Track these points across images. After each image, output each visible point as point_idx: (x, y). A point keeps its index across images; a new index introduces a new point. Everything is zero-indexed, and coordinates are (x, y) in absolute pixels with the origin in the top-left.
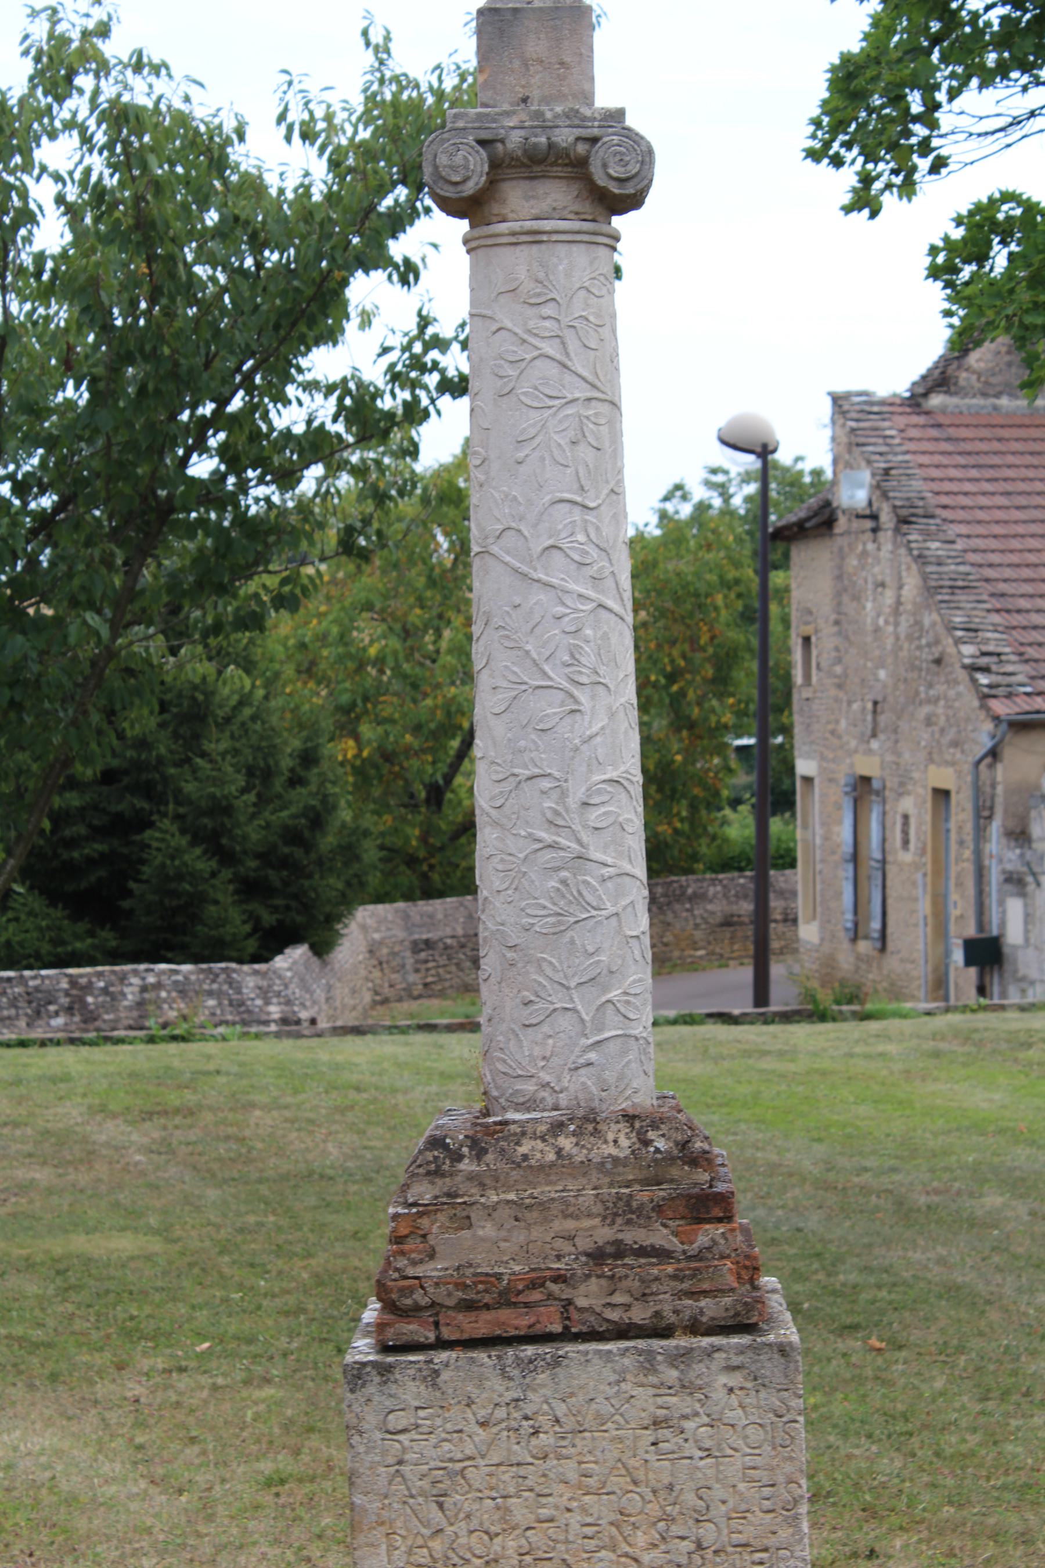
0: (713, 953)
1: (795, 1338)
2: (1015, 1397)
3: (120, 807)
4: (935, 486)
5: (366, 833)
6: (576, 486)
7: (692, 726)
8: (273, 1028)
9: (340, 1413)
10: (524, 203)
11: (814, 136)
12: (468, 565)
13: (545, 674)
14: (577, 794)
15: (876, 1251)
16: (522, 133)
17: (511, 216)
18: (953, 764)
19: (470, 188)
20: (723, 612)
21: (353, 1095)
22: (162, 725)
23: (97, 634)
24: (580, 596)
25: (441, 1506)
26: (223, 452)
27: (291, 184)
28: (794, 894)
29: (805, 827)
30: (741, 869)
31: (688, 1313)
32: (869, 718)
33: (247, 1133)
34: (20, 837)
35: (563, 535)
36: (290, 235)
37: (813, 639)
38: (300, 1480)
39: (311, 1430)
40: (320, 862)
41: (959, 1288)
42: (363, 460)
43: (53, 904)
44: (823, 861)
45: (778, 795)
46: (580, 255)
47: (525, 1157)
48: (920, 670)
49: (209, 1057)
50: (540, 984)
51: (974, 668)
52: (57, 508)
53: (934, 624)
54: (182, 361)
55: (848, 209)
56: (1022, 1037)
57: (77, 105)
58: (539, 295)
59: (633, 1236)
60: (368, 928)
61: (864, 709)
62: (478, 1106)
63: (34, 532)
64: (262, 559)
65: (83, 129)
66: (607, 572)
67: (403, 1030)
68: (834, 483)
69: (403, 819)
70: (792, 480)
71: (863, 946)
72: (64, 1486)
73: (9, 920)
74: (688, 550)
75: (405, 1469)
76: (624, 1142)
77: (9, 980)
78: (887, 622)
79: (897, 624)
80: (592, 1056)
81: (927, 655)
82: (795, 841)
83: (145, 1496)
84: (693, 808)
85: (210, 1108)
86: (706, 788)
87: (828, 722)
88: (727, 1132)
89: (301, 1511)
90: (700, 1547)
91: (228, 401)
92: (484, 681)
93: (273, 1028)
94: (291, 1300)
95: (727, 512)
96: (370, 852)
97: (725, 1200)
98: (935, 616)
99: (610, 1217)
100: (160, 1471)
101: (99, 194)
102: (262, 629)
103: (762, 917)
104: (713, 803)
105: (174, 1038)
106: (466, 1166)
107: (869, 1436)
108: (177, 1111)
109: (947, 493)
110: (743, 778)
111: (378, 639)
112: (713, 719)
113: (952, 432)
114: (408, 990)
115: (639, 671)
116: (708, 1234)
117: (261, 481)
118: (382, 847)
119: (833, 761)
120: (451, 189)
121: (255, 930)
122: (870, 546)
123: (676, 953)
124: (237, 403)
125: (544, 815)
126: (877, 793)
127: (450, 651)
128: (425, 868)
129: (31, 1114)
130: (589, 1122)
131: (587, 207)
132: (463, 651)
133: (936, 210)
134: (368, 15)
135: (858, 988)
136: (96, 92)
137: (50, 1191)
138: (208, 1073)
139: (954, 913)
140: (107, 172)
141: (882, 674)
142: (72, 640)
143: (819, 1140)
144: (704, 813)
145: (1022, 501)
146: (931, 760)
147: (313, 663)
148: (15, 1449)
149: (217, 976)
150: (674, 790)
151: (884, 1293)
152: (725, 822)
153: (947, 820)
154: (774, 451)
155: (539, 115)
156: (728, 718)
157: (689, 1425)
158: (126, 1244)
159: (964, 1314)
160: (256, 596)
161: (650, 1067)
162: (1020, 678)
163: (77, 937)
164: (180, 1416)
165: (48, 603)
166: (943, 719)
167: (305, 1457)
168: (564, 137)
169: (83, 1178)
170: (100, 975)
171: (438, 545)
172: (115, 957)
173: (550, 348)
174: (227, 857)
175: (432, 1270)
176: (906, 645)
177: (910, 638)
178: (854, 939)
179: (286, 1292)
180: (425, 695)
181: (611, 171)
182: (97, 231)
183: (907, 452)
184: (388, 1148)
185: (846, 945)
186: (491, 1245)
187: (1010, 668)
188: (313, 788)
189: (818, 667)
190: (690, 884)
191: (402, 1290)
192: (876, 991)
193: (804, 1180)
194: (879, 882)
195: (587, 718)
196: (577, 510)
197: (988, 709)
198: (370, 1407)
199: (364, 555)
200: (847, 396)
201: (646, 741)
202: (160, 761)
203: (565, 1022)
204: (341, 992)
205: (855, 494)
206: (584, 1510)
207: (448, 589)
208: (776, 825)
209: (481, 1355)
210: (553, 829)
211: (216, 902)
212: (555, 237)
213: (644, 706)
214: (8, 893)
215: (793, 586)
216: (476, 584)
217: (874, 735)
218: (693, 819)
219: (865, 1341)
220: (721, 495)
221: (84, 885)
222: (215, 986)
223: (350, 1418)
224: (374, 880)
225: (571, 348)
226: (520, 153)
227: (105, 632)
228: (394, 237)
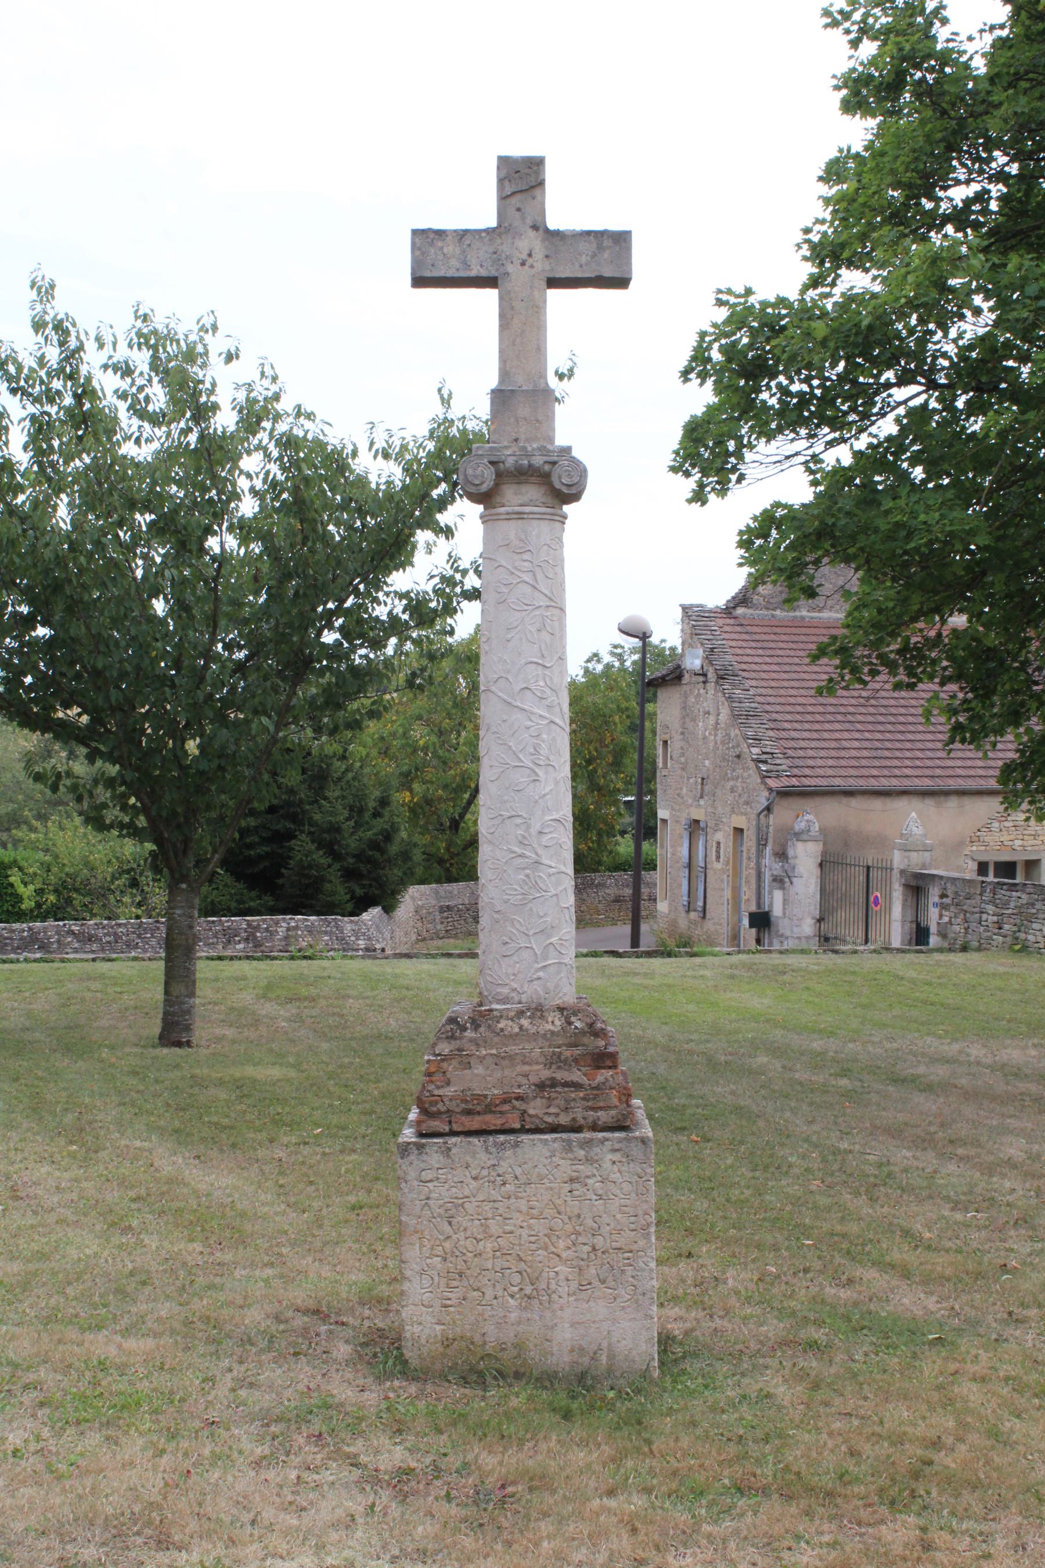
1: (650, 1134)
2: (771, 1170)
3: (278, 827)
4: (739, 659)
5: (415, 845)
7: (599, 789)
8: (361, 953)
9: (395, 1170)
10: (513, 496)
11: (675, 460)
12: (477, 696)
15: (696, 1086)
18: (746, 814)
19: (484, 488)
21: (404, 992)
25: (450, 1223)
26: (341, 629)
29: (662, 847)
30: (625, 870)
31: (590, 1120)
33: (345, 1011)
34: (221, 842)
36: (381, 509)
38: (371, 1207)
39: (377, 1179)
40: (389, 861)
41: (741, 1108)
42: (419, 636)
43: (238, 880)
45: (647, 829)
46: (544, 527)
47: (502, 1030)
49: (324, 969)
52: (248, 658)
55: (690, 501)
56: (781, 968)
57: (263, 436)
59: (561, 1075)
60: (415, 898)
62: (476, 1000)
63: (235, 672)
64: (361, 689)
65: (265, 449)
67: (433, 956)
68: (682, 655)
69: (437, 838)
70: (659, 653)
71: (693, 915)
72: (239, 1206)
75: (431, 1202)
76: (558, 1023)
79: (716, 735)
80: (541, 974)
83: (284, 1213)
84: (599, 835)
85: (325, 997)
86: (606, 823)
88: (615, 1018)
89: (371, 1224)
90: (594, 1249)
91: (345, 601)
92: (485, 762)
93: (361, 953)
94: (368, 1106)
95: (623, 670)
96: (417, 856)
97: (613, 1056)
98: (737, 731)
99: (548, 1065)
100: (293, 1199)
101: (274, 484)
102: (361, 729)
104: (611, 834)
105: (305, 957)
106: (469, 1034)
107: (690, 1190)
108: (306, 998)
110: (628, 819)
115: (572, 757)
116: (603, 1076)
117: (362, 646)
118: (424, 853)
121: (352, 898)
122: (702, 691)
124: (350, 602)
127: (464, 744)
129: (224, 998)
130: (538, 1011)
131: (549, 500)
132: (474, 744)
136: (273, 430)
137: (234, 1041)
138: (323, 978)
139: (744, 898)
140: (279, 473)
141: (707, 763)
142: (253, 732)
143: (666, 1023)
145: (787, 668)
146: (733, 812)
147: (387, 749)
148: (212, 1185)
150: (589, 825)
151: (700, 1110)
152: (617, 843)
155: (524, 448)
156: (620, 785)
157: (590, 1181)
158: (276, 1072)
159: (744, 1122)
161: (573, 981)
163: (252, 899)
164: (304, 1169)
165: (242, 712)
167: (374, 1194)
168: (538, 461)
169: (252, 1035)
172: (272, 911)
174: (336, 856)
175: (449, 1091)
177: (723, 743)
178: (688, 911)
179: (365, 1101)
182: (273, 506)
184: (424, 1022)
185: (683, 914)
186: (482, 1078)
187: (778, 761)
188: (386, 819)
191: (431, 1103)
193: (657, 1045)
198: (411, 1167)
200: (691, 606)
201: (575, 796)
202: (301, 801)
203: (526, 955)
204: (399, 934)
205: (694, 662)
206: (530, 1227)
207: (465, 710)
208: (646, 846)
209: (474, 1140)
213: (574, 778)
216: (482, 708)
217: (702, 797)
218: (599, 842)
219: (689, 1136)
221: (256, 870)
223: (400, 1173)
224: (419, 871)
227: (272, 728)
228: (440, 511)
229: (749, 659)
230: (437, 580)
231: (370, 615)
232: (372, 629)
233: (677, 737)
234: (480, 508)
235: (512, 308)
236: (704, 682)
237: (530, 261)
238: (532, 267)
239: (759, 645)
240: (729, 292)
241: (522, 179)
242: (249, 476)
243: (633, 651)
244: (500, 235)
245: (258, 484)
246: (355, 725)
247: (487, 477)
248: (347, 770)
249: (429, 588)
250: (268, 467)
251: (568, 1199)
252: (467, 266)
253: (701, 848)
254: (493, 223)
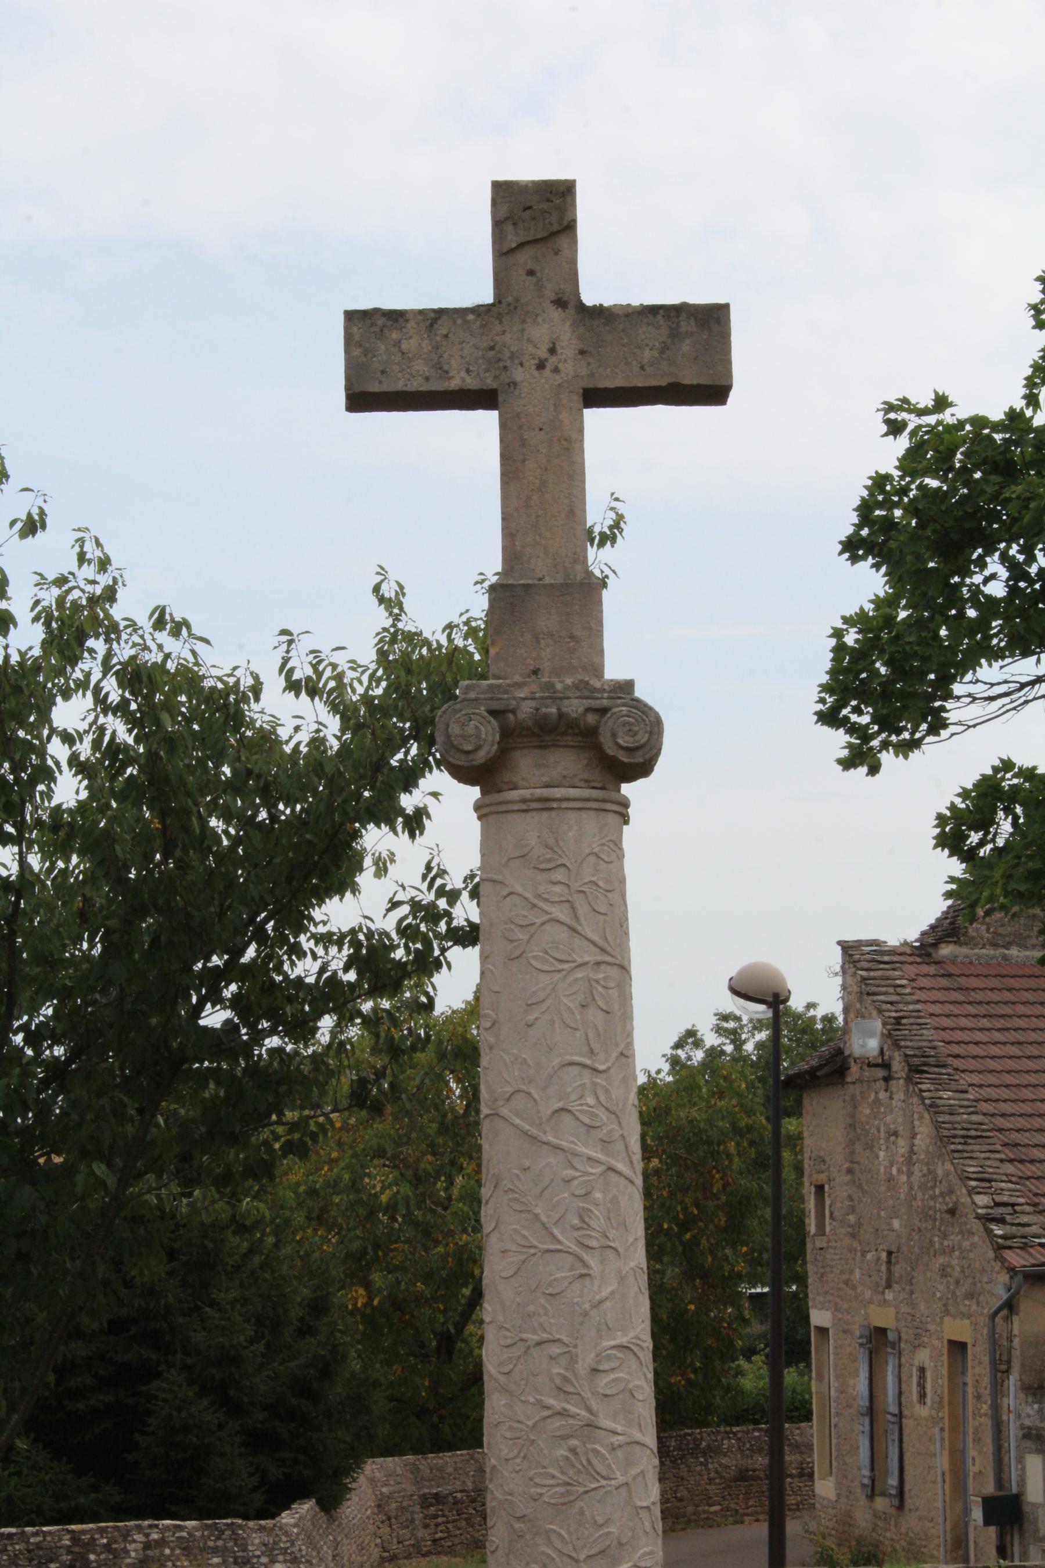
0: (728, 1509)
4: (946, 1035)
5: (376, 1384)
6: (585, 1049)
10: (533, 771)
13: (554, 1237)
14: (586, 1360)
16: (533, 704)
17: (522, 783)
18: (969, 1316)
19: (481, 757)
20: (736, 1159)
22: (171, 1274)
23: (104, 1183)
24: (590, 1159)
26: (235, 1003)
27: (304, 737)
28: (810, 1447)
30: (755, 1422)
32: (884, 1268)
35: (573, 1097)
37: (827, 1187)
42: (375, 1010)
44: (837, 1414)
45: (793, 1345)
46: (590, 822)
48: (935, 1220)
50: (548, 1556)
51: (987, 1219)
53: (947, 1174)
54: (196, 914)
57: (89, 666)
58: (549, 860)
60: (378, 1480)
61: (879, 1258)
63: (45, 1083)
66: (617, 1135)
68: (846, 1030)
70: (803, 1026)
71: (881, 1503)
73: (11, 1475)
74: (701, 1098)
77: (10, 1536)
78: (899, 1170)
79: (910, 1174)
81: (940, 1205)
82: (810, 1394)
87: (842, 1272)
91: (242, 952)
98: (948, 1166)
101: (114, 751)
102: (271, 1177)
103: (777, 1471)
104: (727, 1353)
109: (958, 1043)
111: (390, 1186)
112: (727, 1267)
113: (963, 981)
114: (417, 1546)
117: (272, 1032)
118: (392, 1399)
119: (848, 1312)
120: (463, 757)
122: (882, 1095)
123: (690, 1509)
125: (552, 1380)
126: (893, 1345)
127: (461, 1198)
128: (435, 1419)
132: (474, 1199)
133: (942, 769)
134: (382, 571)
135: (877, 1546)
139: (973, 1470)
141: (896, 1224)
142: (79, 1190)
144: (717, 1363)
146: (947, 1312)
147: (324, 1210)
149: (223, 1532)
152: (740, 1372)
153: (964, 1373)
154: (787, 999)
155: (549, 686)
156: (741, 1267)
160: (266, 1143)
162: (1035, 1229)
166: (958, 1269)
168: (574, 707)
170: (103, 1531)
171: (451, 1090)
173: (559, 913)
176: (919, 1195)
177: (923, 1187)
178: (871, 1497)
180: (437, 1243)
181: (620, 741)
183: (918, 1001)
185: (863, 1501)
187: (1025, 1219)
189: (831, 1217)
190: (704, 1436)
192: (894, 1550)
194: (896, 1437)
195: (596, 1282)
196: (586, 1073)
197: (1003, 1261)
199: (377, 1110)
200: (859, 944)
205: (866, 1042)
208: (790, 1376)
210: (562, 1396)
211: (222, 1455)
212: (565, 805)
214: (11, 1448)
215: (806, 1134)
217: (889, 1286)
220: (733, 1042)
222: (220, 1543)
225: (581, 912)
226: (530, 723)
227: (112, 1182)
229: (965, 1036)
230: (405, 909)
231: (286, 976)
232: (290, 1000)
233: (841, 1178)
234: (474, 793)
235: (523, 443)
236: (887, 1079)
237: (553, 360)
238: (556, 370)
239: (982, 1010)
240: (905, 404)
241: (535, 219)
242: (68, 738)
243: (758, 1025)
244: (500, 317)
245: (85, 749)
246: (263, 1170)
247: (487, 735)
248: (251, 1251)
249: (389, 924)
250: (102, 720)
252: (445, 374)
253: (890, 1378)
254: (487, 297)
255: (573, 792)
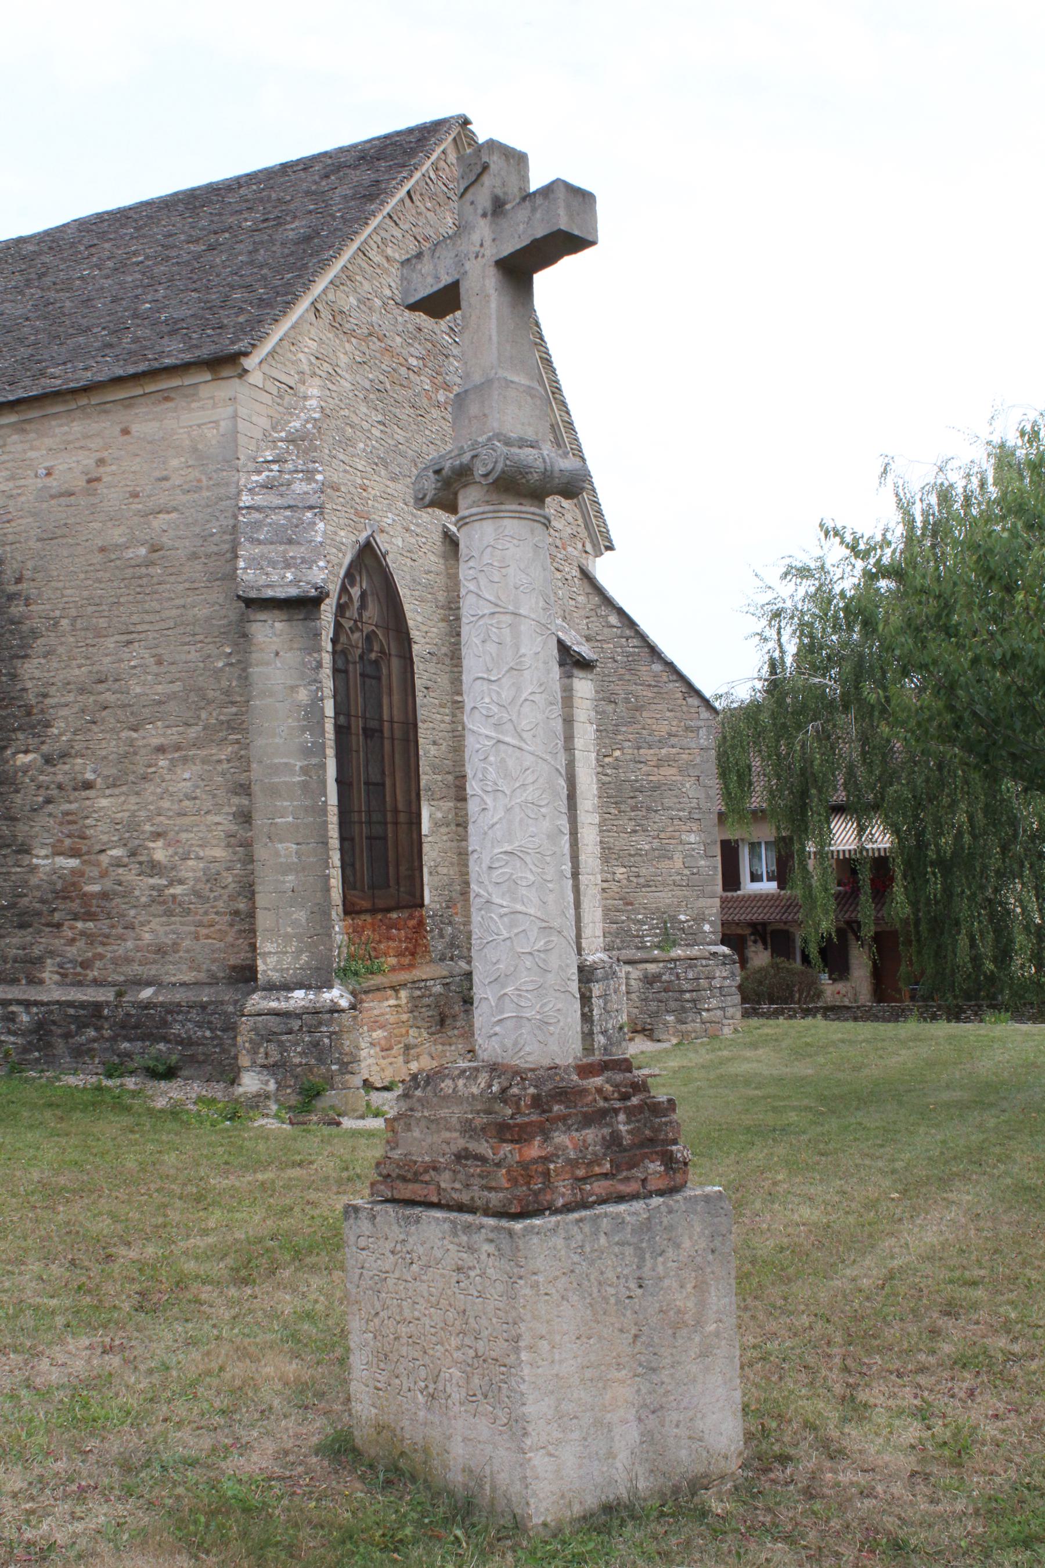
80: (497, 1029)
99: (463, 1132)
251: (457, 1291)
255: (474, 510)
